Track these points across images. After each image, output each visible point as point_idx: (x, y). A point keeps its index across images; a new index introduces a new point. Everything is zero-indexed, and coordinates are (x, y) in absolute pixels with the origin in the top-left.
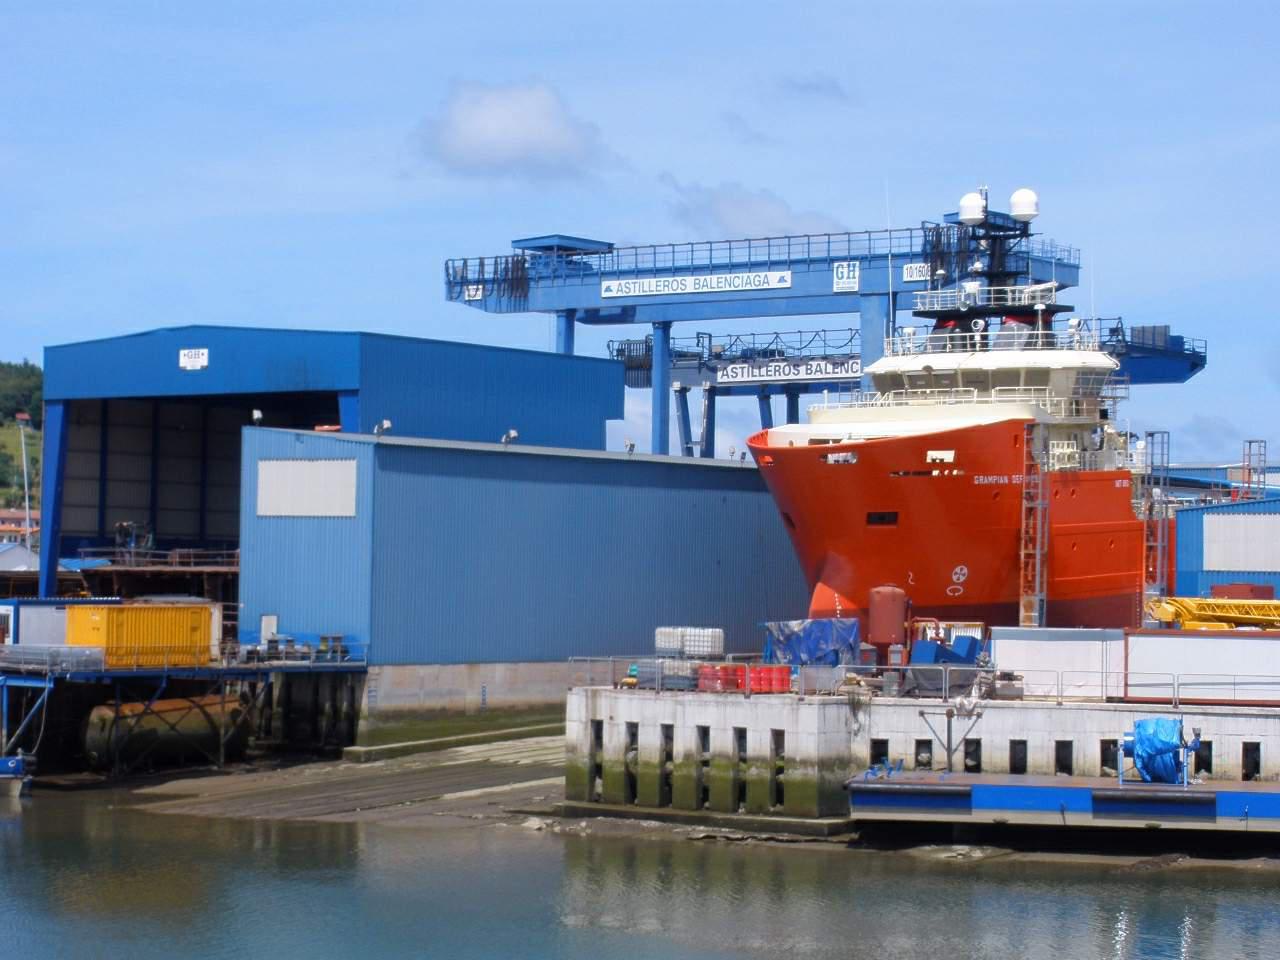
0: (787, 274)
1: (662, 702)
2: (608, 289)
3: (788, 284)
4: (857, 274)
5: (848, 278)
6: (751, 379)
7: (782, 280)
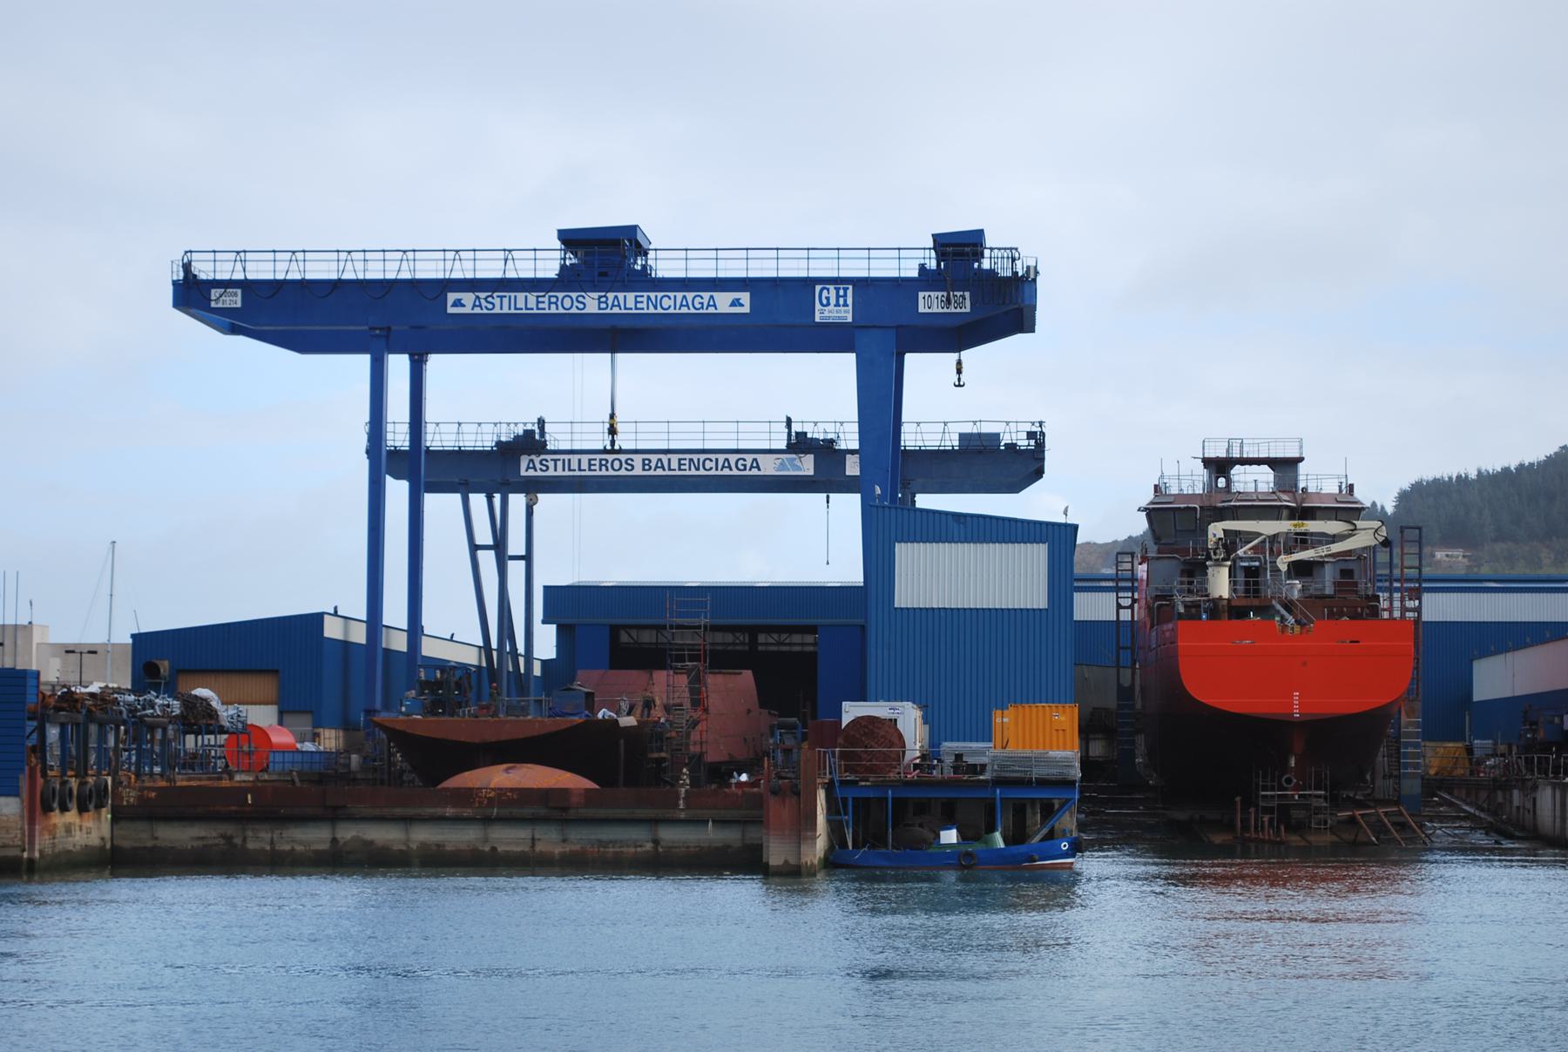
0: (745, 297)
1: (762, 892)
2: (458, 303)
3: (746, 309)
4: (850, 301)
5: (837, 305)
6: (567, 473)
7: (736, 303)
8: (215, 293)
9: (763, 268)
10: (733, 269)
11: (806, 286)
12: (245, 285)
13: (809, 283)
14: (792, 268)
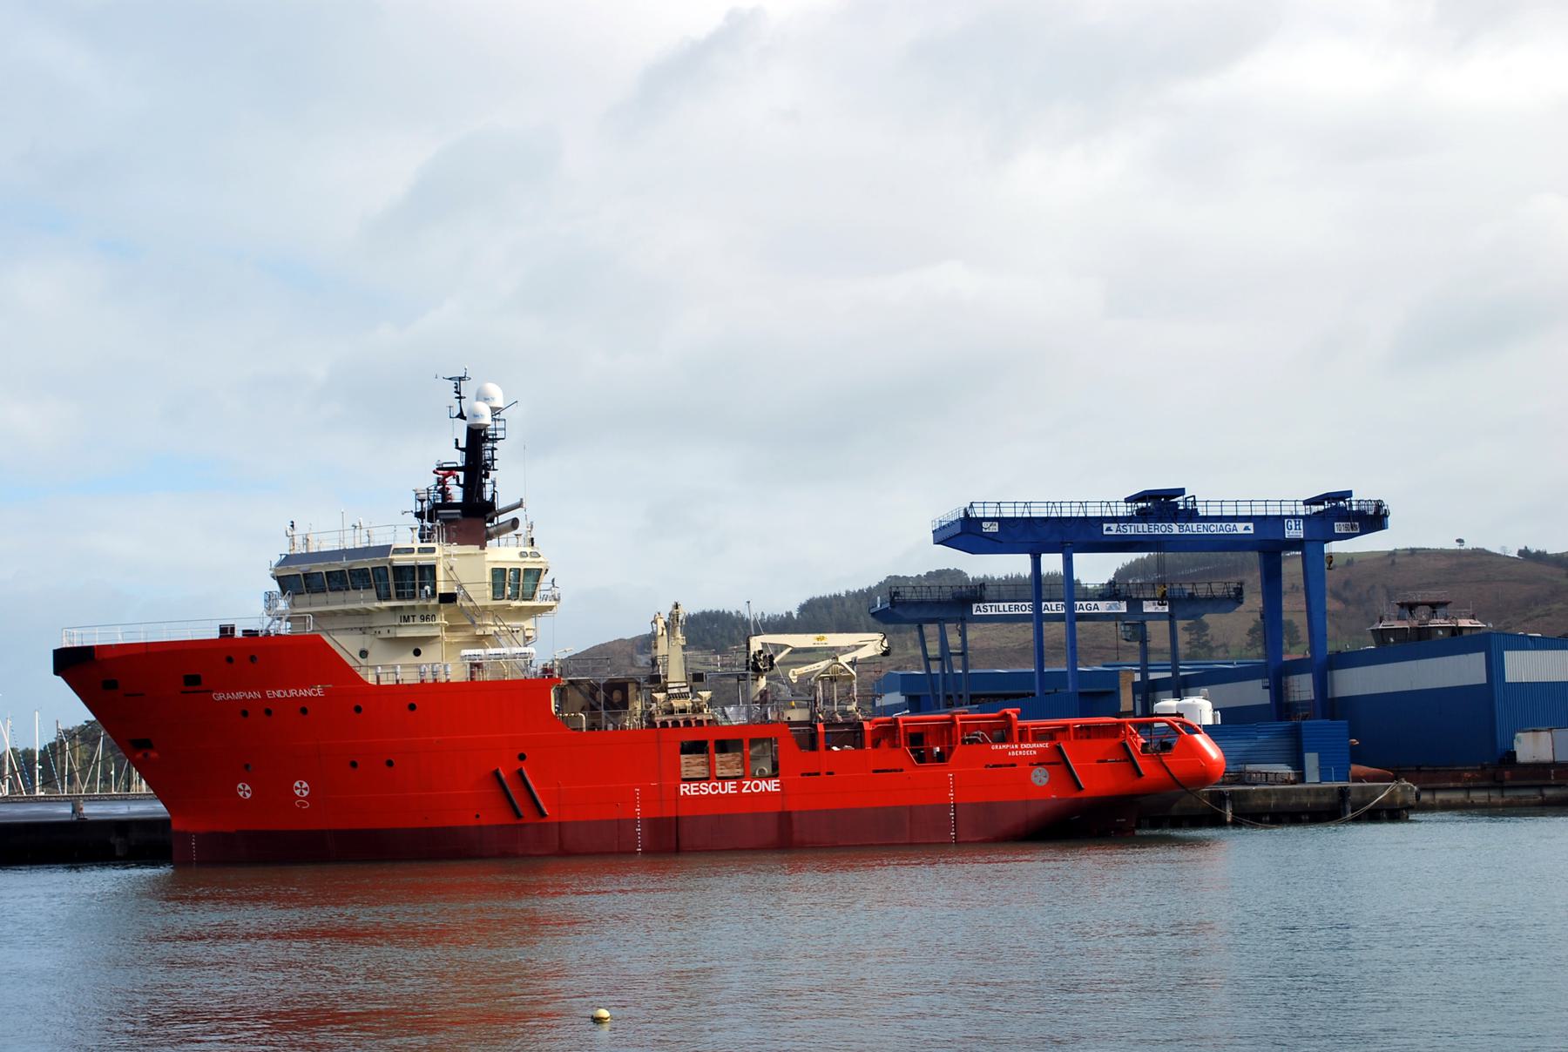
0: (1251, 525)
8: (985, 525)
9: (1259, 511)
10: (1244, 511)
11: (1280, 519)
12: (1001, 521)
13: (1281, 518)
14: (1274, 511)
